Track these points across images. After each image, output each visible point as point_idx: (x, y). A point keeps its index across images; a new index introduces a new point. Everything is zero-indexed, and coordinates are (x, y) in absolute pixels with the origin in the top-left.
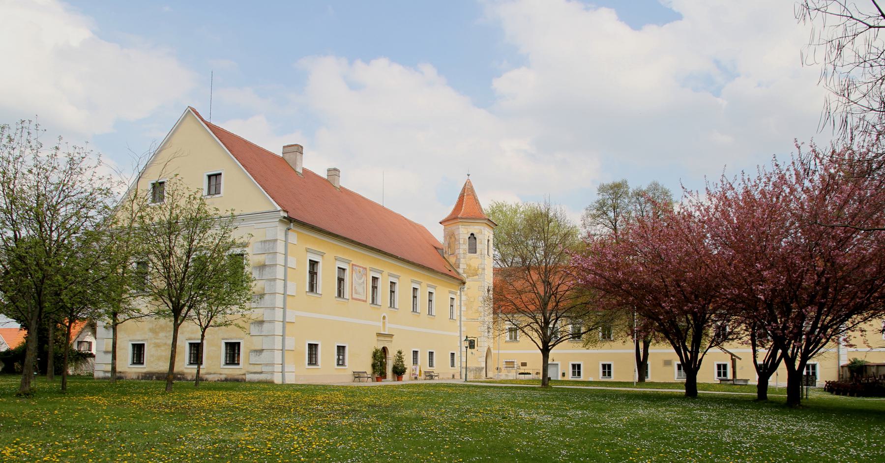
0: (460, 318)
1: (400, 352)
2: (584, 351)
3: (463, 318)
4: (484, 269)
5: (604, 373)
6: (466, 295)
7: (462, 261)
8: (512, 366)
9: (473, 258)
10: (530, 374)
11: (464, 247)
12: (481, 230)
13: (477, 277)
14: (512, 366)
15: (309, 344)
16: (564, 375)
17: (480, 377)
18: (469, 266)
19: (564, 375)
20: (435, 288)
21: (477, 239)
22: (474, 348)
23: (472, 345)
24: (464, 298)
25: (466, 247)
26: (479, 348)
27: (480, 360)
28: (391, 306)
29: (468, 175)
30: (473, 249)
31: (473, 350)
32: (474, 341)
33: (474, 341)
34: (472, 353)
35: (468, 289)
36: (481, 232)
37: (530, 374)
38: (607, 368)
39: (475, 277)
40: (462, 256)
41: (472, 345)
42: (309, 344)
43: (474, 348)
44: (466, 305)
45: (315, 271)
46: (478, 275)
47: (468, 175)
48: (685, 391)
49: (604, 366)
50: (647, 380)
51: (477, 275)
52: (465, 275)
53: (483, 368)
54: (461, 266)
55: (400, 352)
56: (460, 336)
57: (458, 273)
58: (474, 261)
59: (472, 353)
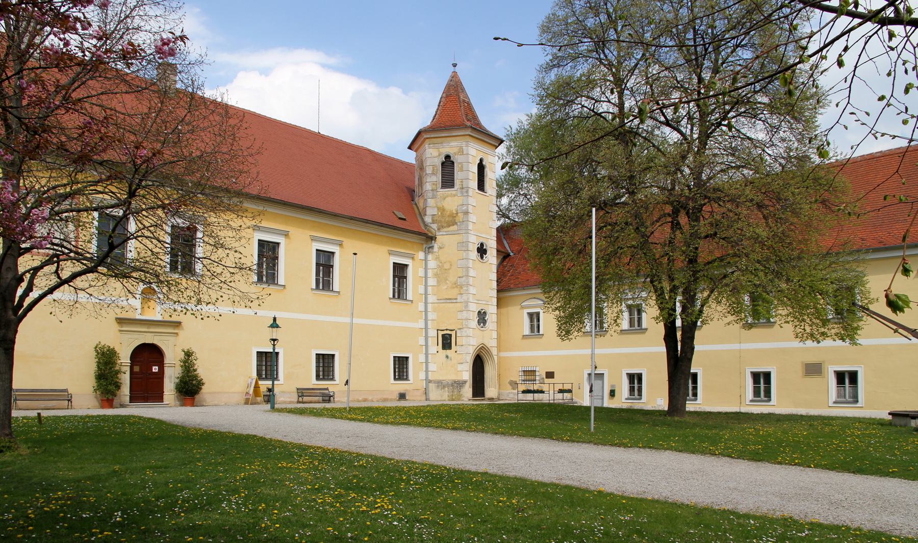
0: (426, 298)
1: (188, 354)
2: (796, 344)
3: (431, 299)
4: (466, 213)
5: (757, 393)
6: (437, 258)
7: (431, 202)
8: (532, 377)
9: (448, 196)
10: (542, 392)
11: (433, 179)
12: (461, 148)
13: (455, 228)
14: (532, 377)
15: (258, 352)
16: (612, 393)
17: (460, 397)
18: (442, 210)
19: (612, 393)
20: (413, 258)
21: (455, 164)
22: (450, 348)
23: (447, 342)
24: (432, 264)
25: (438, 178)
26: (458, 348)
27: (460, 367)
28: (394, 296)
29: (455, 65)
30: (448, 181)
31: (448, 352)
32: (450, 335)
33: (450, 335)
34: (447, 357)
35: (440, 248)
36: (461, 152)
37: (542, 392)
38: (762, 380)
39: (452, 228)
40: (430, 195)
41: (447, 342)
42: (258, 352)
43: (450, 348)
44: (436, 275)
45: (332, 264)
46: (456, 223)
47: (455, 65)
48: (15, 413)
49: (756, 376)
50: (690, 406)
51: (455, 223)
52: (435, 226)
53: (465, 382)
54: (429, 212)
55: (188, 354)
56: (426, 328)
57: (426, 225)
58: (450, 200)
59: (447, 357)
